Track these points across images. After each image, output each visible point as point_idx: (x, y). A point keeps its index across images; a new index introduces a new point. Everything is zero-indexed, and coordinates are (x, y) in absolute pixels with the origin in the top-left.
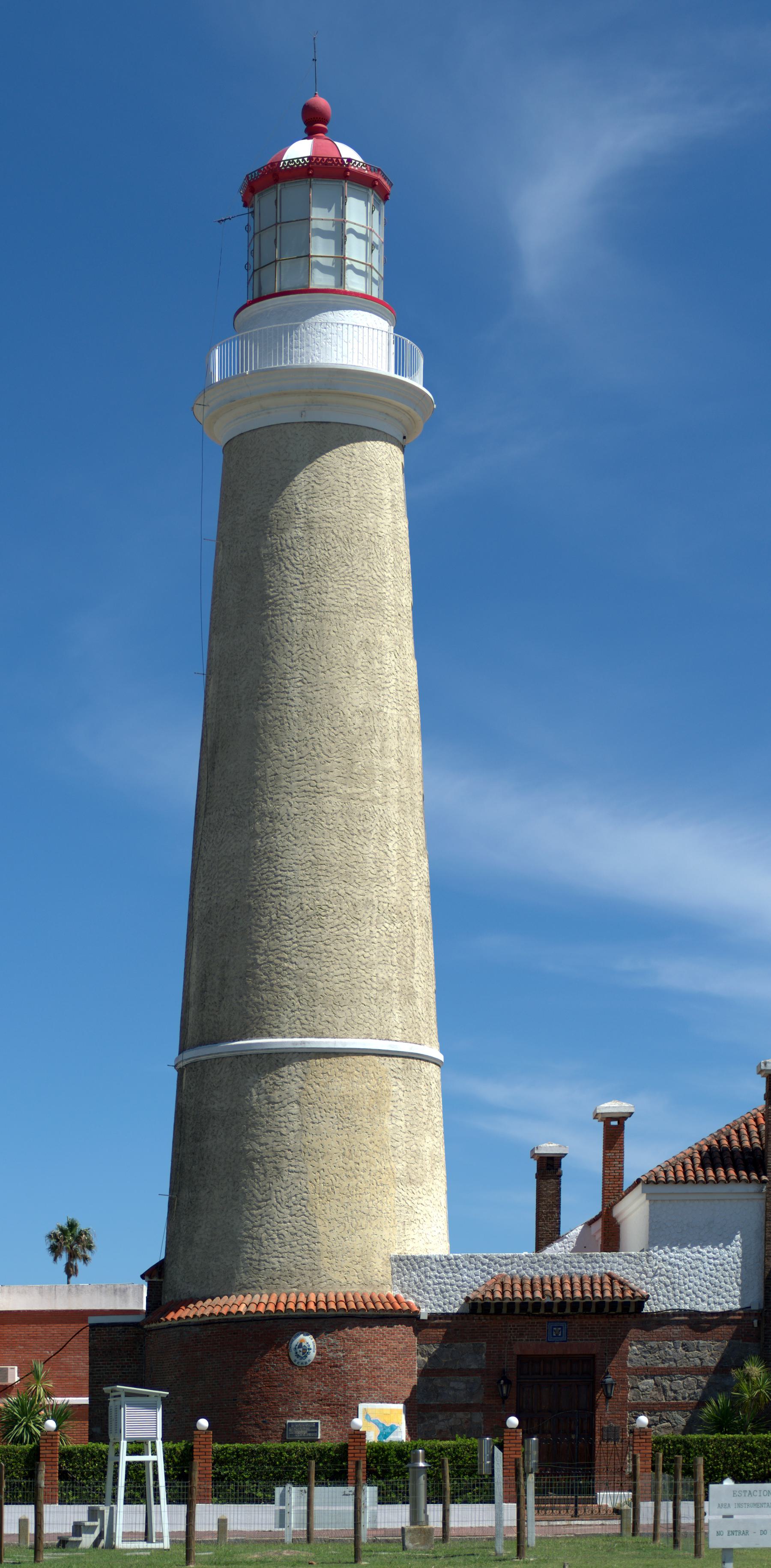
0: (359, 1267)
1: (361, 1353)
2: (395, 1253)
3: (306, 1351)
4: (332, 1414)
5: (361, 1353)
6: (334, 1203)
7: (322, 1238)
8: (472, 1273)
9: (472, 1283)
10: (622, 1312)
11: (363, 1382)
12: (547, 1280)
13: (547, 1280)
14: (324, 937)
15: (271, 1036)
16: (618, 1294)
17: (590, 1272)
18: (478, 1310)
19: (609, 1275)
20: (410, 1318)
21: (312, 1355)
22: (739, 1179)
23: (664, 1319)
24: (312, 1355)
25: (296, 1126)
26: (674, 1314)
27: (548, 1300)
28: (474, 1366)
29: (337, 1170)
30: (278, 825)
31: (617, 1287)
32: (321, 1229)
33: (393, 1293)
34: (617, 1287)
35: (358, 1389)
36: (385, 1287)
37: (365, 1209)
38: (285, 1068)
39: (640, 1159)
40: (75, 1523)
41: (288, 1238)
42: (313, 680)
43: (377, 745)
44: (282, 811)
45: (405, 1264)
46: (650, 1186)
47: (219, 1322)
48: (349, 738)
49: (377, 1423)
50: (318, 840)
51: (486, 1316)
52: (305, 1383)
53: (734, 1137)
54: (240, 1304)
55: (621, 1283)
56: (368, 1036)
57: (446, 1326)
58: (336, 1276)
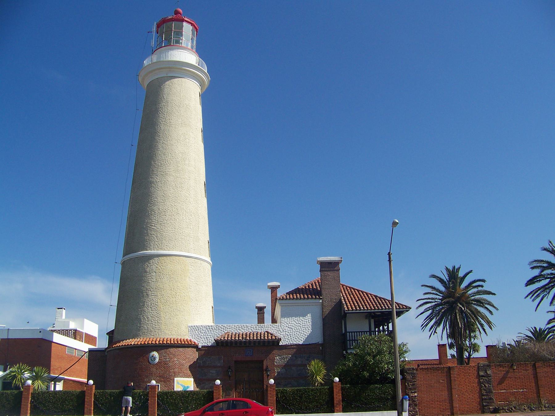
0: (176, 329)
1: (175, 359)
2: (190, 325)
3: (155, 359)
4: (164, 381)
5: (175, 359)
6: (167, 306)
7: (162, 318)
8: (217, 331)
9: (218, 334)
10: (271, 344)
11: (176, 370)
12: (244, 334)
13: (244, 334)
14: (166, 219)
15: (147, 250)
16: (270, 338)
17: (260, 331)
18: (220, 345)
19: (267, 332)
20: (196, 346)
21: (157, 360)
22: (312, 298)
23: (285, 347)
24: (157, 360)
25: (154, 280)
26: (291, 346)
27: (244, 340)
28: (219, 365)
29: (169, 295)
30: (153, 185)
31: (269, 335)
32: (162, 315)
33: (189, 339)
34: (269, 335)
35: (174, 373)
36: (185, 335)
37: (179, 309)
38: (151, 261)
39: (280, 293)
40: (191, 367)
41: (150, 318)
42: (166, 143)
43: (187, 162)
44: (154, 181)
45: (193, 328)
46: (284, 301)
47: (130, 347)
48: (178, 160)
49: (182, 385)
50: (166, 189)
51: (222, 346)
52: (154, 370)
53: (311, 286)
54: (132, 342)
55: (271, 334)
56: (181, 251)
57: (205, 350)
58: (167, 332)
